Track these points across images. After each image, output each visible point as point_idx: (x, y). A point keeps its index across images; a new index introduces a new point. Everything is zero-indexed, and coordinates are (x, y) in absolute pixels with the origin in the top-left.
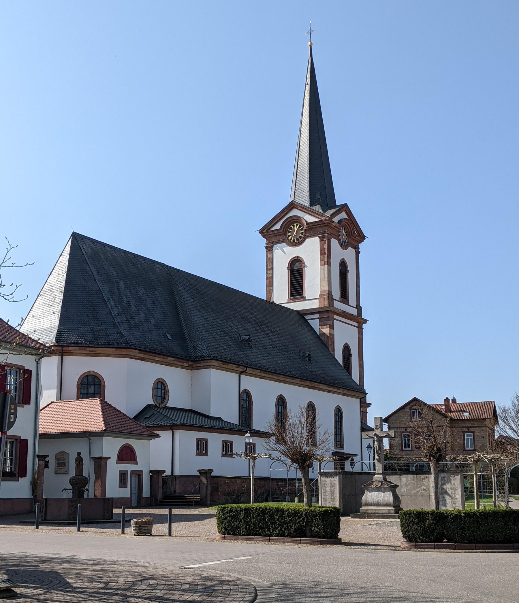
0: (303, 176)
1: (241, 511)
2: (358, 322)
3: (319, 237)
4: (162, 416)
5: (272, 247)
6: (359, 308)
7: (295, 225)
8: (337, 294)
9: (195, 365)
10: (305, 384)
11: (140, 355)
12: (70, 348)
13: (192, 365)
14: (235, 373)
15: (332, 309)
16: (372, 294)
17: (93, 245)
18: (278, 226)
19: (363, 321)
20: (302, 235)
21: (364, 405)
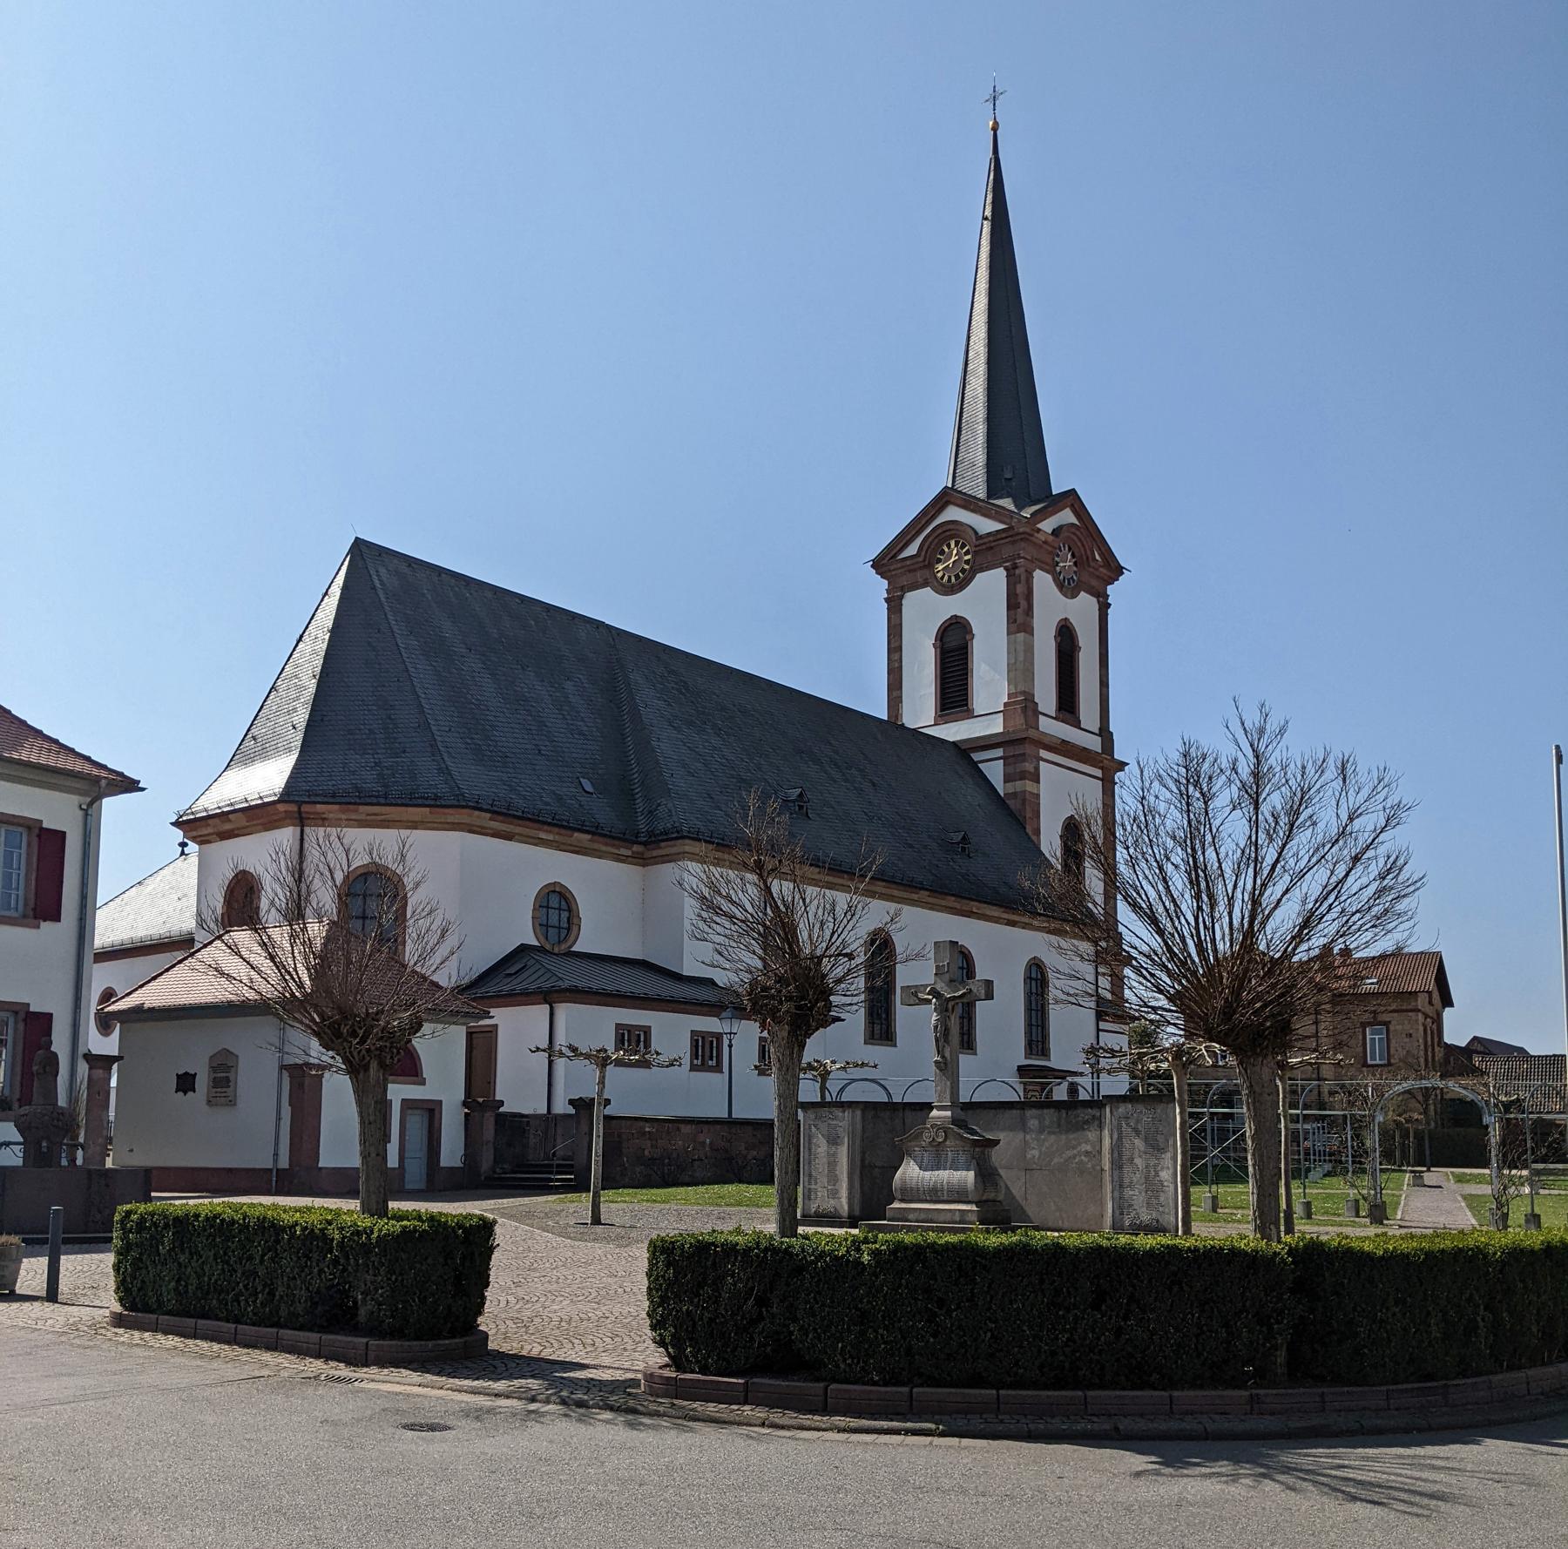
0: (974, 431)
1: (166, 1226)
5: (902, 597)
6: (1105, 734)
7: (953, 544)
8: (1046, 695)
9: (648, 854)
10: (943, 903)
11: (495, 825)
15: (1032, 733)
17: (407, 570)
18: (912, 549)
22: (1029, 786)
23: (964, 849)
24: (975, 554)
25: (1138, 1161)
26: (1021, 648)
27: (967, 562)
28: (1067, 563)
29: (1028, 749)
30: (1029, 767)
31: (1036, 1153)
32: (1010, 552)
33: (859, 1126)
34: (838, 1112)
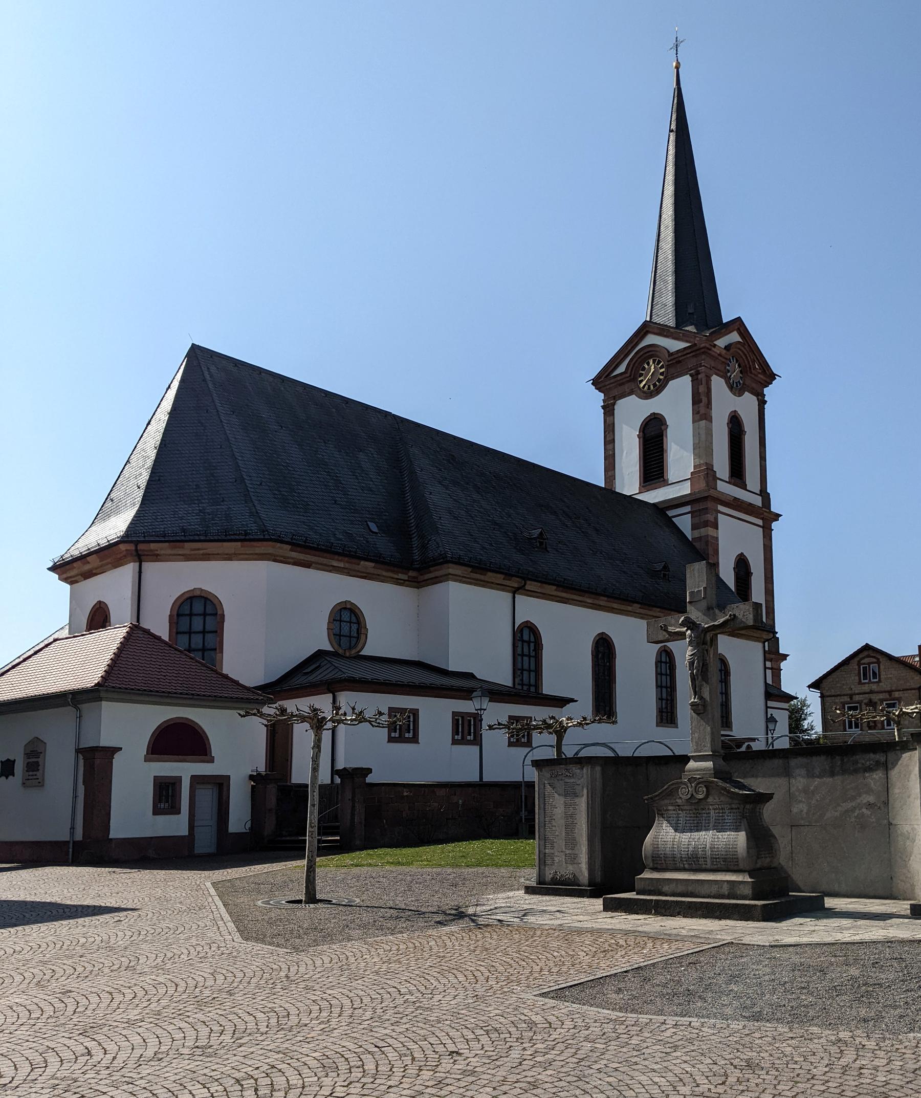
0: (666, 282)
2: (762, 519)
3: (691, 375)
4: (332, 668)
5: (614, 404)
6: (764, 494)
7: (651, 362)
8: (722, 467)
9: (421, 578)
12: (153, 546)
13: (414, 577)
14: (503, 590)
15: (712, 492)
16: (787, 476)
18: (622, 369)
19: (772, 516)
20: (661, 377)
21: (774, 657)
22: (710, 531)
23: (665, 575)
24: (668, 367)
26: (703, 432)
27: (662, 374)
28: (735, 374)
29: (709, 504)
30: (710, 517)
31: (803, 807)
32: (695, 363)
33: (599, 784)
34: (575, 769)
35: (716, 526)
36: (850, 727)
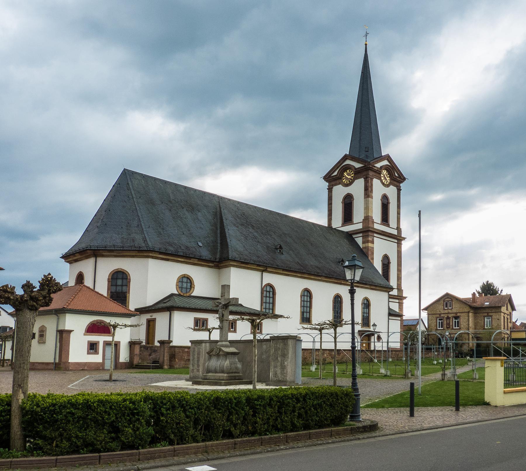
5: (332, 188)
6: (399, 229)
18: (335, 173)
22: (370, 245)
24: (355, 174)
25: (279, 359)
29: (370, 234)
31: (265, 356)
35: (373, 242)
36: (455, 327)
